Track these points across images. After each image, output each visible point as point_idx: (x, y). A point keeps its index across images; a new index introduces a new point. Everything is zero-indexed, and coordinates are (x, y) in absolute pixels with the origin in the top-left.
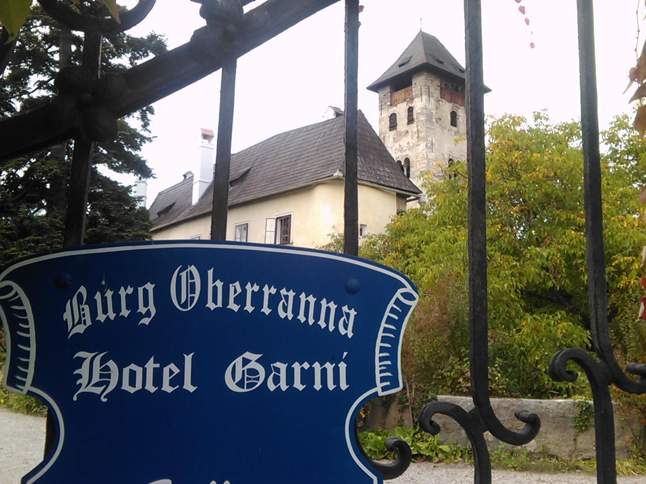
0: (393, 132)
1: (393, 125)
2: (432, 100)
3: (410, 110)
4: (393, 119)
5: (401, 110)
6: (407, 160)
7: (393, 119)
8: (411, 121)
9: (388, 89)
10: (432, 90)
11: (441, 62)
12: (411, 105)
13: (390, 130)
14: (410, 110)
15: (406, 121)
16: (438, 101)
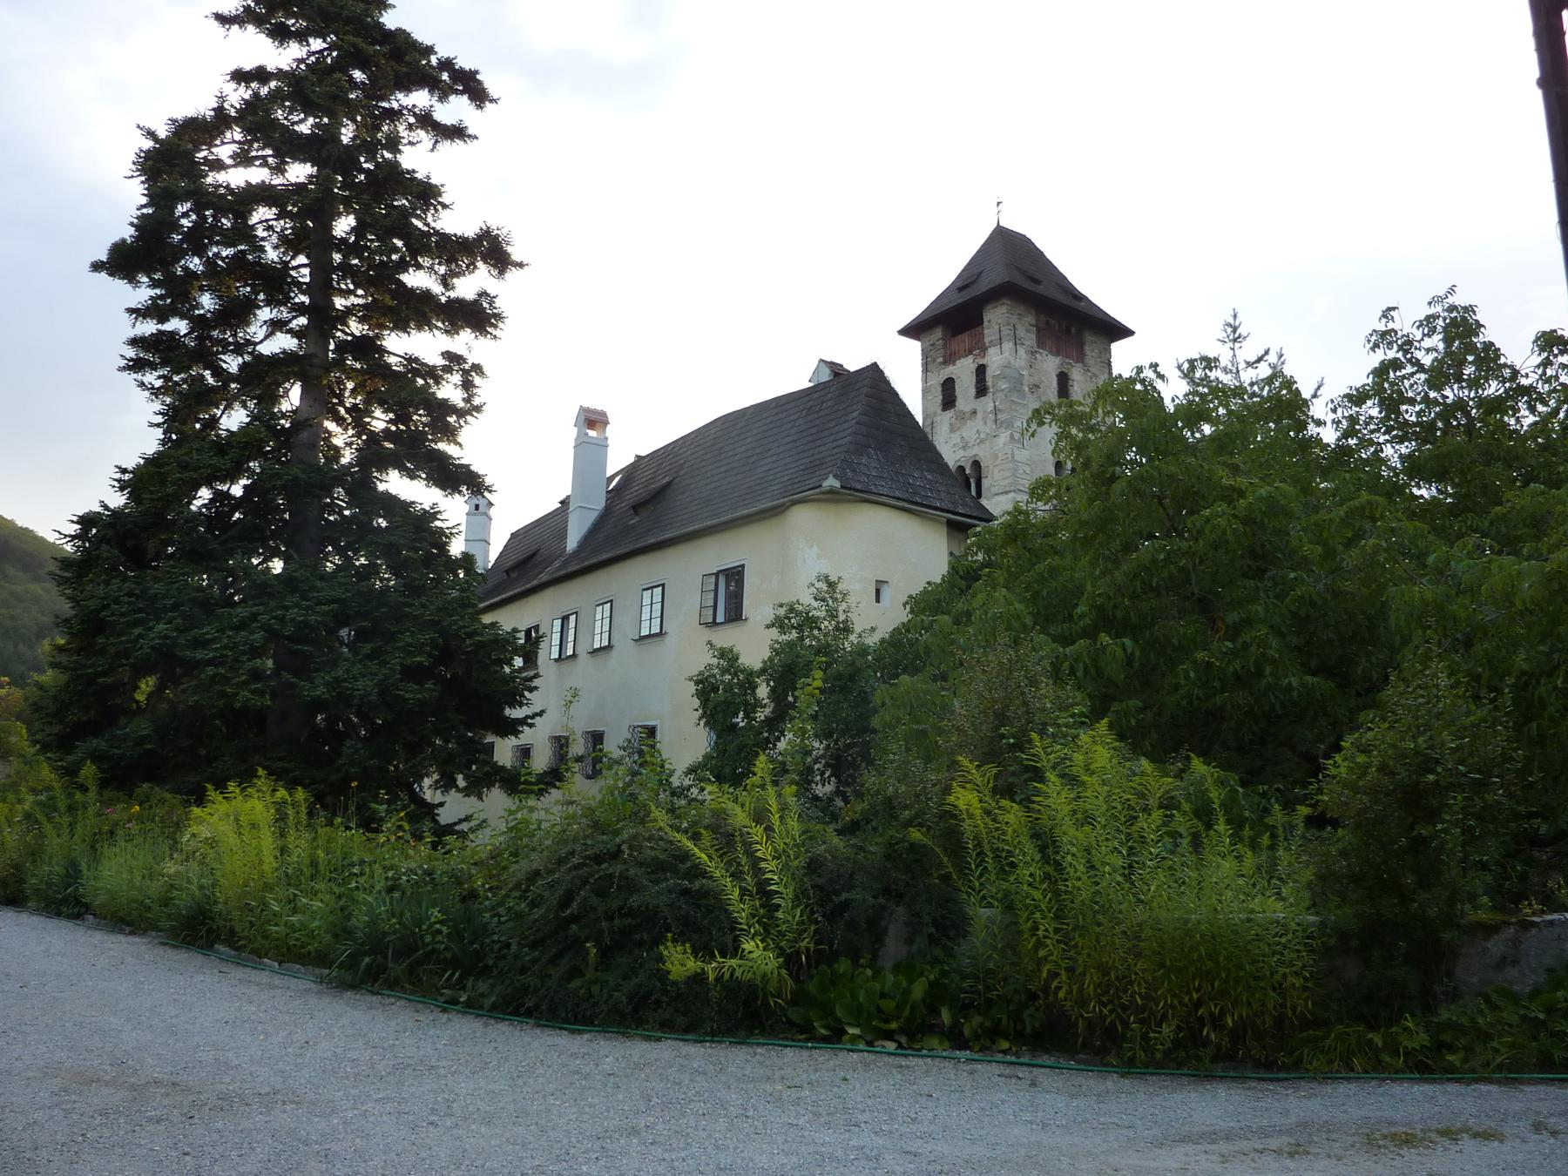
0: (950, 413)
1: (949, 401)
2: (1022, 351)
3: (981, 371)
4: (948, 387)
5: (964, 370)
6: (976, 465)
7: (948, 387)
8: (981, 390)
9: (938, 333)
10: (1021, 332)
11: (1037, 282)
12: (981, 362)
13: (944, 410)
14: (981, 371)
15: (973, 391)
16: (1033, 353)
